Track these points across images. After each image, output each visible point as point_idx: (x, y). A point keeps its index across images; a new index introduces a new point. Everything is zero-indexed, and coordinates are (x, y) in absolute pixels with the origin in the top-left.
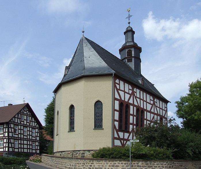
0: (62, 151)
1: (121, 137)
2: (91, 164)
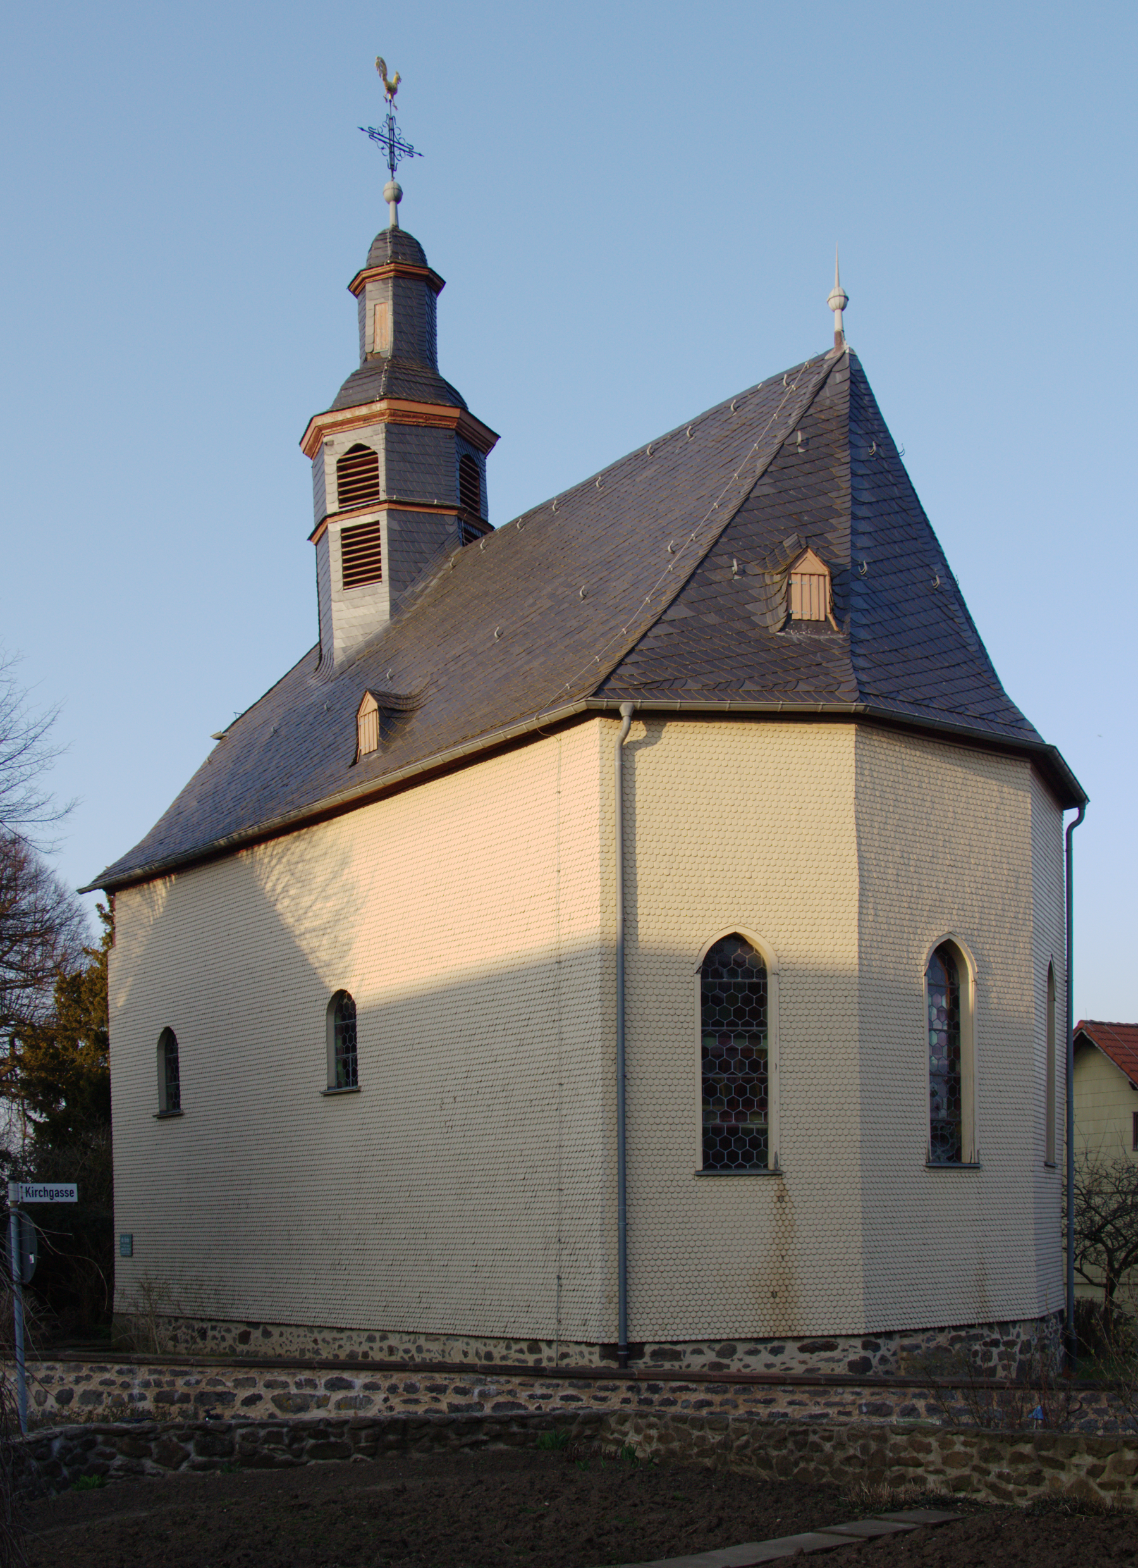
0: (878, 1335)
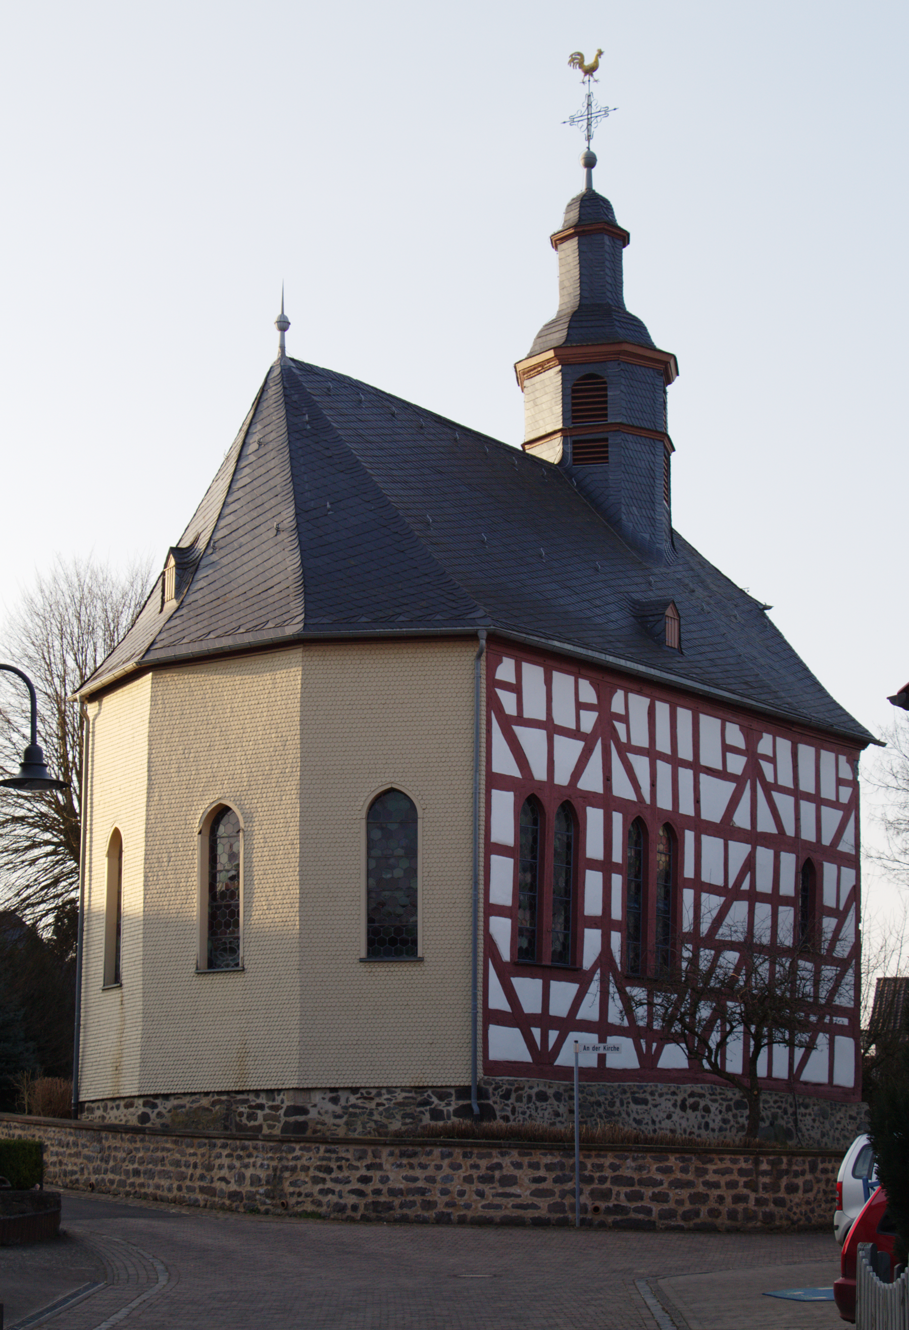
0: (156, 1096)
1: (531, 1003)
2: (368, 1167)
